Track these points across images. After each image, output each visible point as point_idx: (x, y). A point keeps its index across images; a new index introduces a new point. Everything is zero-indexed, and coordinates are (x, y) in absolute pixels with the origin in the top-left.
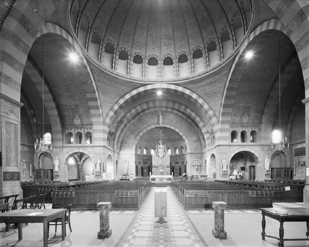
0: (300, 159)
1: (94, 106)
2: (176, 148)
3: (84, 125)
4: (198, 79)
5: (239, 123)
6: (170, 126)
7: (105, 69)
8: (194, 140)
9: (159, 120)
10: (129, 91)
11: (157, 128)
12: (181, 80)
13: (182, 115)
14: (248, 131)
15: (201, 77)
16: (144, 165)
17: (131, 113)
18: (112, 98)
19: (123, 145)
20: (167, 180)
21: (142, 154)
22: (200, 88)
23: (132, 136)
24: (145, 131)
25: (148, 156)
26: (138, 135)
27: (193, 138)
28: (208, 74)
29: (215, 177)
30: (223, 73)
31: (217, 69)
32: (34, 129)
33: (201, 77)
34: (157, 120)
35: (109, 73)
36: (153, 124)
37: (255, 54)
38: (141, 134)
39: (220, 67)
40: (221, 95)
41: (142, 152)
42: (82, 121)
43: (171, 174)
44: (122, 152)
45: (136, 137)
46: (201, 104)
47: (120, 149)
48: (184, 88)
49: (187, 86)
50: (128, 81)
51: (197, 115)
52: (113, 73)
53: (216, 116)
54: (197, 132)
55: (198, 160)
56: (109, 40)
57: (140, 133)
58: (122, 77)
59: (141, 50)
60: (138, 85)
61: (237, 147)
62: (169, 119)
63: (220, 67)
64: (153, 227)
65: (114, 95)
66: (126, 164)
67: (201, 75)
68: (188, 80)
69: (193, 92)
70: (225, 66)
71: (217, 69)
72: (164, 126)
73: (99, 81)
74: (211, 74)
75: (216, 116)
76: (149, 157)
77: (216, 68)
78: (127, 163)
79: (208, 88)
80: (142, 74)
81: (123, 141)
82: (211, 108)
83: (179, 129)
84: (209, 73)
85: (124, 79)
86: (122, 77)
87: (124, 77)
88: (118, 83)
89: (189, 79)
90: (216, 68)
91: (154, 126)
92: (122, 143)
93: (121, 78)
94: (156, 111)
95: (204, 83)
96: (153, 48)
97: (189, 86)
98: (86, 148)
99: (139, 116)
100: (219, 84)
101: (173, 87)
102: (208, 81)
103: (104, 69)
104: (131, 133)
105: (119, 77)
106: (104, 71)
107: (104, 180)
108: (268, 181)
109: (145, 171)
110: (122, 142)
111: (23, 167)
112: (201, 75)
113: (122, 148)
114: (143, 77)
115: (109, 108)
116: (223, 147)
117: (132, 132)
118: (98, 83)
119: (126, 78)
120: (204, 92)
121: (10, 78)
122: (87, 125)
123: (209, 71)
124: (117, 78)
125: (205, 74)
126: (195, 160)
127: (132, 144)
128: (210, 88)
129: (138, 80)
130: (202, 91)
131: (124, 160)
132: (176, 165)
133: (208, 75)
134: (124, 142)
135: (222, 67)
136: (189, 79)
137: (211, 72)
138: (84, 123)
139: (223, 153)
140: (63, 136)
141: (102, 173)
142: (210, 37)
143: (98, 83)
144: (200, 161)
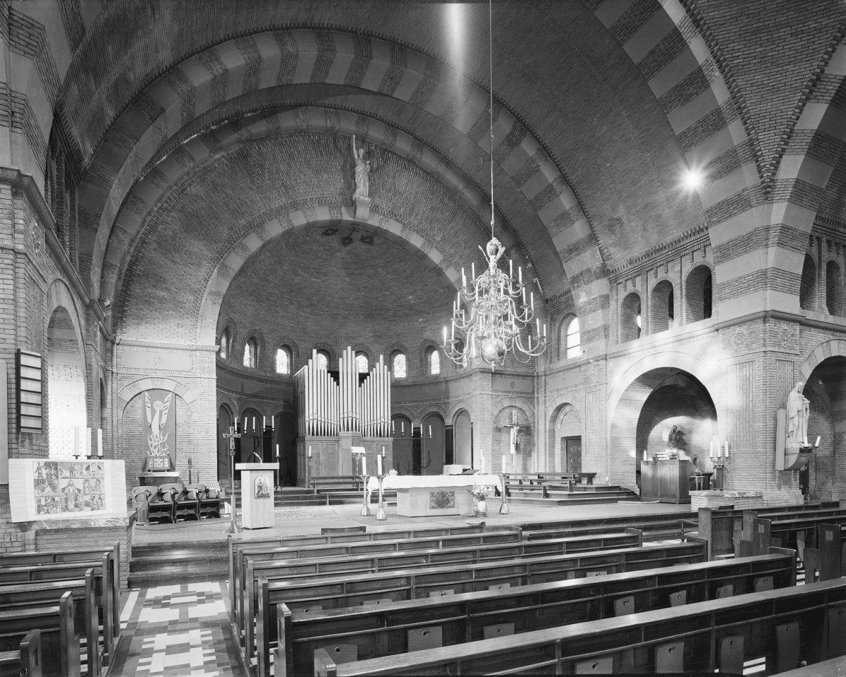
2: (397, 352)
6: (405, 226)
9: (351, 186)
11: (331, 229)
13: (461, 186)
17: (218, 70)
19: (136, 289)
21: (234, 365)
23: (197, 246)
24: (275, 229)
25: (261, 380)
26: (231, 244)
29: (159, 515)
34: (340, 184)
36: (322, 202)
38: (254, 243)
44: (130, 334)
46: (700, 69)
47: (121, 314)
51: (564, 179)
53: (756, 157)
55: (519, 404)
57: (245, 235)
62: (397, 193)
66: (158, 405)
72: (374, 221)
75: (756, 157)
76: (268, 386)
81: (139, 269)
82: (739, 109)
83: (442, 251)
91: (323, 215)
92: (128, 279)
94: (333, 134)
99: (244, 133)
104: (188, 229)
109: (278, 454)
110: (130, 270)
113: (132, 309)
117: (196, 223)
126: (507, 403)
127: (197, 293)
134: (147, 275)
144: (525, 408)
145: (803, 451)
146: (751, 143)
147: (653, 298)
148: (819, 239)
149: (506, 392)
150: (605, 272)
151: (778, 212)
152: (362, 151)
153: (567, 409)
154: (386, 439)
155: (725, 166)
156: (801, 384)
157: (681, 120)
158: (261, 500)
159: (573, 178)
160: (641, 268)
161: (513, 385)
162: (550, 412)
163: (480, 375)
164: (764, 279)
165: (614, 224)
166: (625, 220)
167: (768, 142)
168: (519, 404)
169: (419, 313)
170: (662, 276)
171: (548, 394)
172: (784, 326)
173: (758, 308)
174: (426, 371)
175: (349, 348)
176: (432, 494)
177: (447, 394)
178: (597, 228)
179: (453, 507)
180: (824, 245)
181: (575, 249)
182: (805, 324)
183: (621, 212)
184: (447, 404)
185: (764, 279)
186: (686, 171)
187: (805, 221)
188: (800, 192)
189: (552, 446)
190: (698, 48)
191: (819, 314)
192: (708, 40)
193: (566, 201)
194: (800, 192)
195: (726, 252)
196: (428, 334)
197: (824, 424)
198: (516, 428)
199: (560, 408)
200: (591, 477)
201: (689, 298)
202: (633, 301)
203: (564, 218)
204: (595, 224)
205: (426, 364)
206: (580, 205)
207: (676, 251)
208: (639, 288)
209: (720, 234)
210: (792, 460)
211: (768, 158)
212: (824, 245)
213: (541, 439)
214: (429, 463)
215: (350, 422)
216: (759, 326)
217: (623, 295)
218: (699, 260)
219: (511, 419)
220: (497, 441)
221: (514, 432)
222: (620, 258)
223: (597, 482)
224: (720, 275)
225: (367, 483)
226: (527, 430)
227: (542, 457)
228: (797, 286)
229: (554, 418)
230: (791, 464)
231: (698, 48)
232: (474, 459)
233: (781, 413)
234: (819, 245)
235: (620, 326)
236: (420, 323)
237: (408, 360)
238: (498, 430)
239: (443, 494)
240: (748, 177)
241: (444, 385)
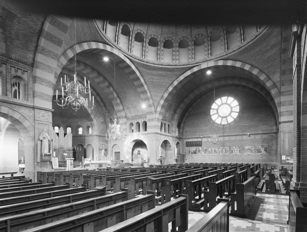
0: (190, 149)
1: (55, 38)
3: (12, 59)
4: (151, 66)
8: (101, 121)
10: (89, 39)
12: (136, 59)
14: (167, 123)
15: (154, 65)
20: (131, 167)
22: (149, 75)
27: (100, 119)
28: (162, 66)
30: (175, 73)
31: (173, 67)
33: (154, 65)
37: (206, 73)
39: (176, 67)
40: (164, 89)
42: (8, 50)
49: (139, 68)
53: (154, 106)
54: (103, 114)
63: (176, 67)
64: (261, 207)
67: (155, 64)
68: (142, 62)
69: (141, 76)
70: (181, 68)
71: (173, 67)
74: (165, 68)
77: (171, 66)
79: (156, 78)
80: (116, 30)
84: (163, 66)
89: (143, 61)
90: (172, 66)
95: (155, 72)
97: (141, 69)
98: (16, 108)
100: (167, 80)
102: (160, 72)
112: (155, 64)
120: (151, 80)
122: (18, 61)
123: (164, 65)
125: (159, 65)
126: (102, 143)
128: (158, 80)
130: (150, 79)
132: (79, 149)
133: (162, 68)
135: (177, 68)
136: (143, 61)
137: (166, 67)
138: (13, 56)
142: (169, 35)
144: (106, 145)
145: (161, 156)
146: (153, 103)
147: (136, 125)
148: (163, 119)
149: (101, 140)
150: (126, 117)
151: (157, 116)
152: (69, 79)
153: (116, 145)
154: (71, 151)
155: (150, 106)
156: (160, 145)
157: (142, 96)
158: (72, 166)
159: (120, 97)
160: (133, 118)
161: (103, 139)
162: (112, 146)
163: (95, 137)
164: (155, 127)
165: (128, 108)
166: (131, 108)
167: (156, 104)
168: (104, 144)
169: (77, 118)
170: (138, 121)
171: (111, 141)
172: (158, 135)
173: (155, 132)
174: (78, 133)
175: (62, 127)
176: (99, 165)
177: (85, 140)
178: (125, 108)
179: (102, 167)
180: (164, 120)
181: (119, 111)
182: (161, 134)
183: (130, 106)
184: (85, 142)
185: (155, 127)
186: (142, 105)
187: (161, 117)
188: (160, 113)
189: (112, 154)
190: (146, 87)
191: (163, 132)
192: (147, 86)
193: (118, 101)
194: (160, 113)
195: (149, 120)
196: (79, 123)
197: (164, 151)
198: (104, 149)
199: (114, 145)
200: (122, 161)
201: (143, 126)
202: (132, 124)
203: (117, 104)
204: (124, 107)
205: (77, 131)
206: (121, 102)
207: (140, 117)
208: (133, 122)
209: (149, 117)
210: (159, 158)
211: (156, 106)
212: (164, 120)
213: (109, 152)
214: (78, 157)
215: (61, 147)
216: (154, 135)
217: (129, 123)
218: (144, 120)
219: (102, 147)
220: (99, 153)
221: (103, 150)
222: (129, 115)
223: (124, 162)
224: (148, 124)
225: (84, 162)
226: (106, 150)
227: (110, 157)
228: (160, 128)
229: (113, 147)
230: (159, 159)
231: (146, 87)
232: (94, 156)
233: (158, 150)
234: (163, 120)
235: (129, 129)
236: (77, 120)
237: (72, 130)
238: (100, 150)
239: (101, 165)
240: (153, 109)
241: (83, 137)
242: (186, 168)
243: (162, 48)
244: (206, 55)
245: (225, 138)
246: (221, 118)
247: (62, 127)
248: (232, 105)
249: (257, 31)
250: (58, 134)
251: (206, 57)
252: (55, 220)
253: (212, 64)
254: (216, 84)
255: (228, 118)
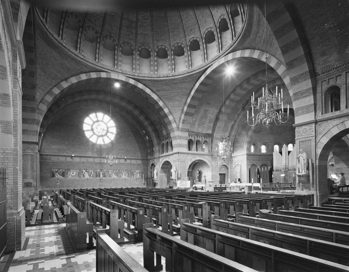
5: (341, 66)
7: (159, 77)
10: (192, 86)
16: (261, 169)
18: (178, 101)
19: (235, 145)
32: (148, 145)
35: (164, 78)
41: (258, 149)
43: (259, 182)
45: (247, 132)
48: (243, 50)
50: (186, 76)
52: (168, 77)
56: (159, 46)
58: (179, 75)
59: (194, 33)
60: (197, 75)
61: (336, 122)
65: (180, 97)
68: (240, 37)
73: (158, 91)
78: (239, 168)
85: (181, 76)
86: (179, 75)
87: (181, 74)
88: (177, 83)
93: (178, 77)
96: (205, 21)
101: (132, 82)
103: (158, 77)
105: (176, 77)
106: (158, 80)
107: (179, 188)
108: (70, 191)
111: (136, 176)
114: (206, 61)
115: (180, 112)
116: (304, 127)
118: (158, 93)
119: (184, 74)
121: (26, 130)
124: (175, 79)
129: (196, 70)
131: (236, 164)
139: (303, 140)
140: (159, 148)
141: (177, 180)
143: (158, 93)
175: (284, 144)
242: (80, 191)
243: (138, 57)
244: (169, 70)
245: (59, 158)
246: (96, 137)
247: (284, 144)
248: (91, 123)
249: (219, 52)
250: (289, 152)
251: (170, 72)
252: (78, 253)
253: (123, 78)
254: (117, 101)
255: (94, 135)
